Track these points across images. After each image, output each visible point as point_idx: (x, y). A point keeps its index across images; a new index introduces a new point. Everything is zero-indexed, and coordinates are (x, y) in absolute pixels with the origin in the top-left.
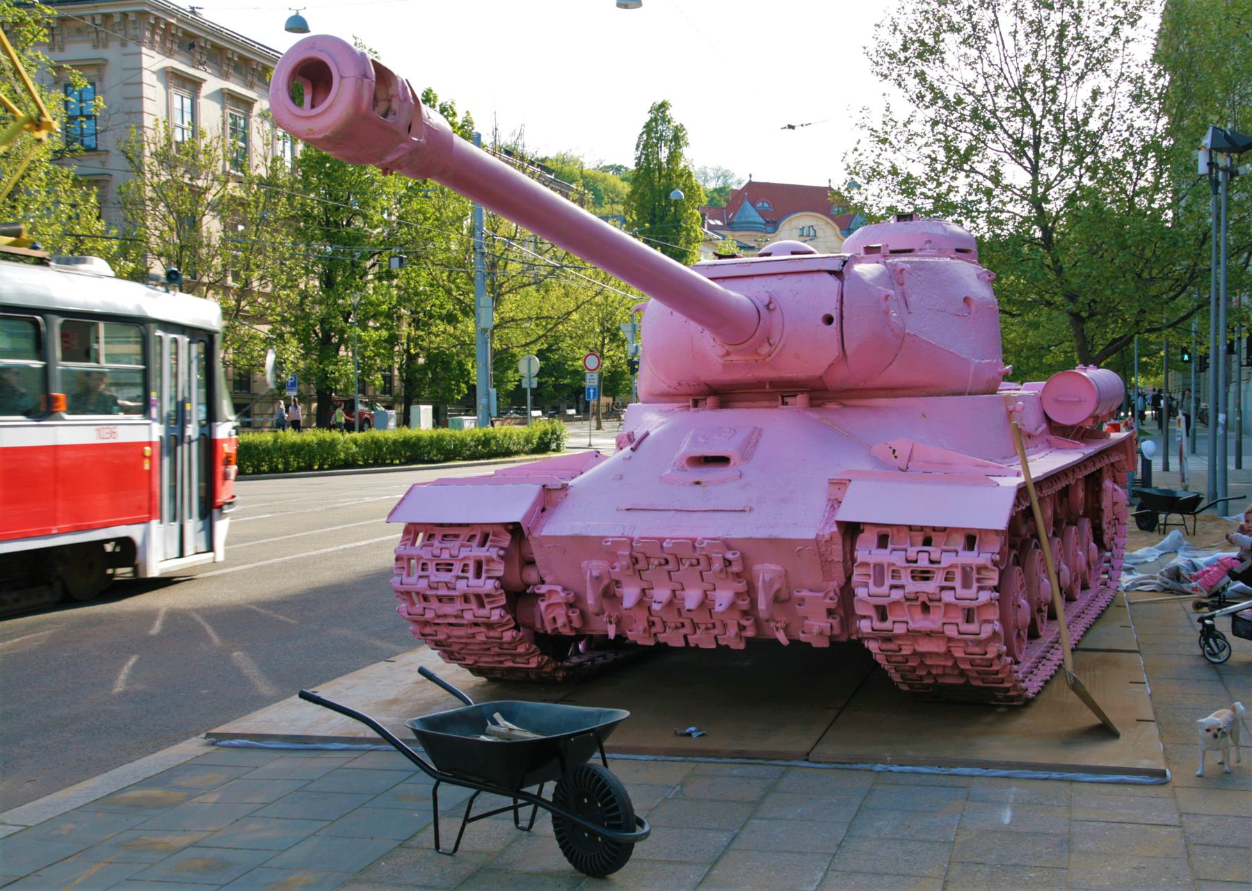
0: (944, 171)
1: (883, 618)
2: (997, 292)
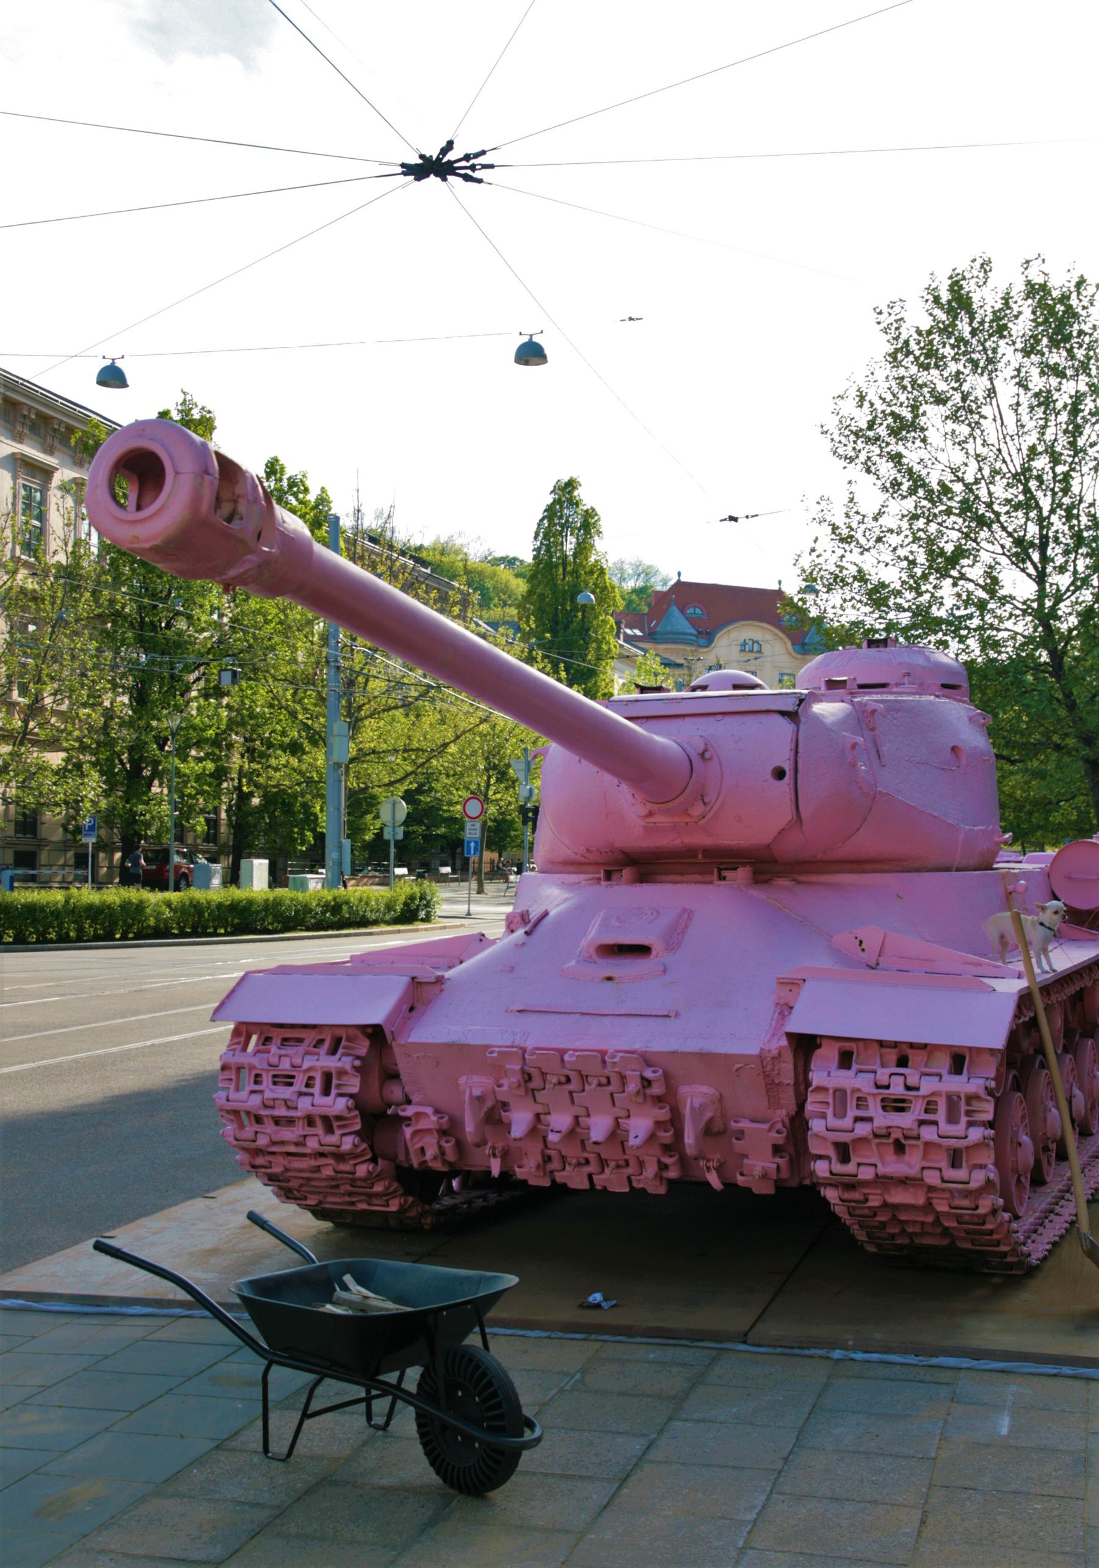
0: (925, 577)
1: (845, 1159)
2: (992, 732)
